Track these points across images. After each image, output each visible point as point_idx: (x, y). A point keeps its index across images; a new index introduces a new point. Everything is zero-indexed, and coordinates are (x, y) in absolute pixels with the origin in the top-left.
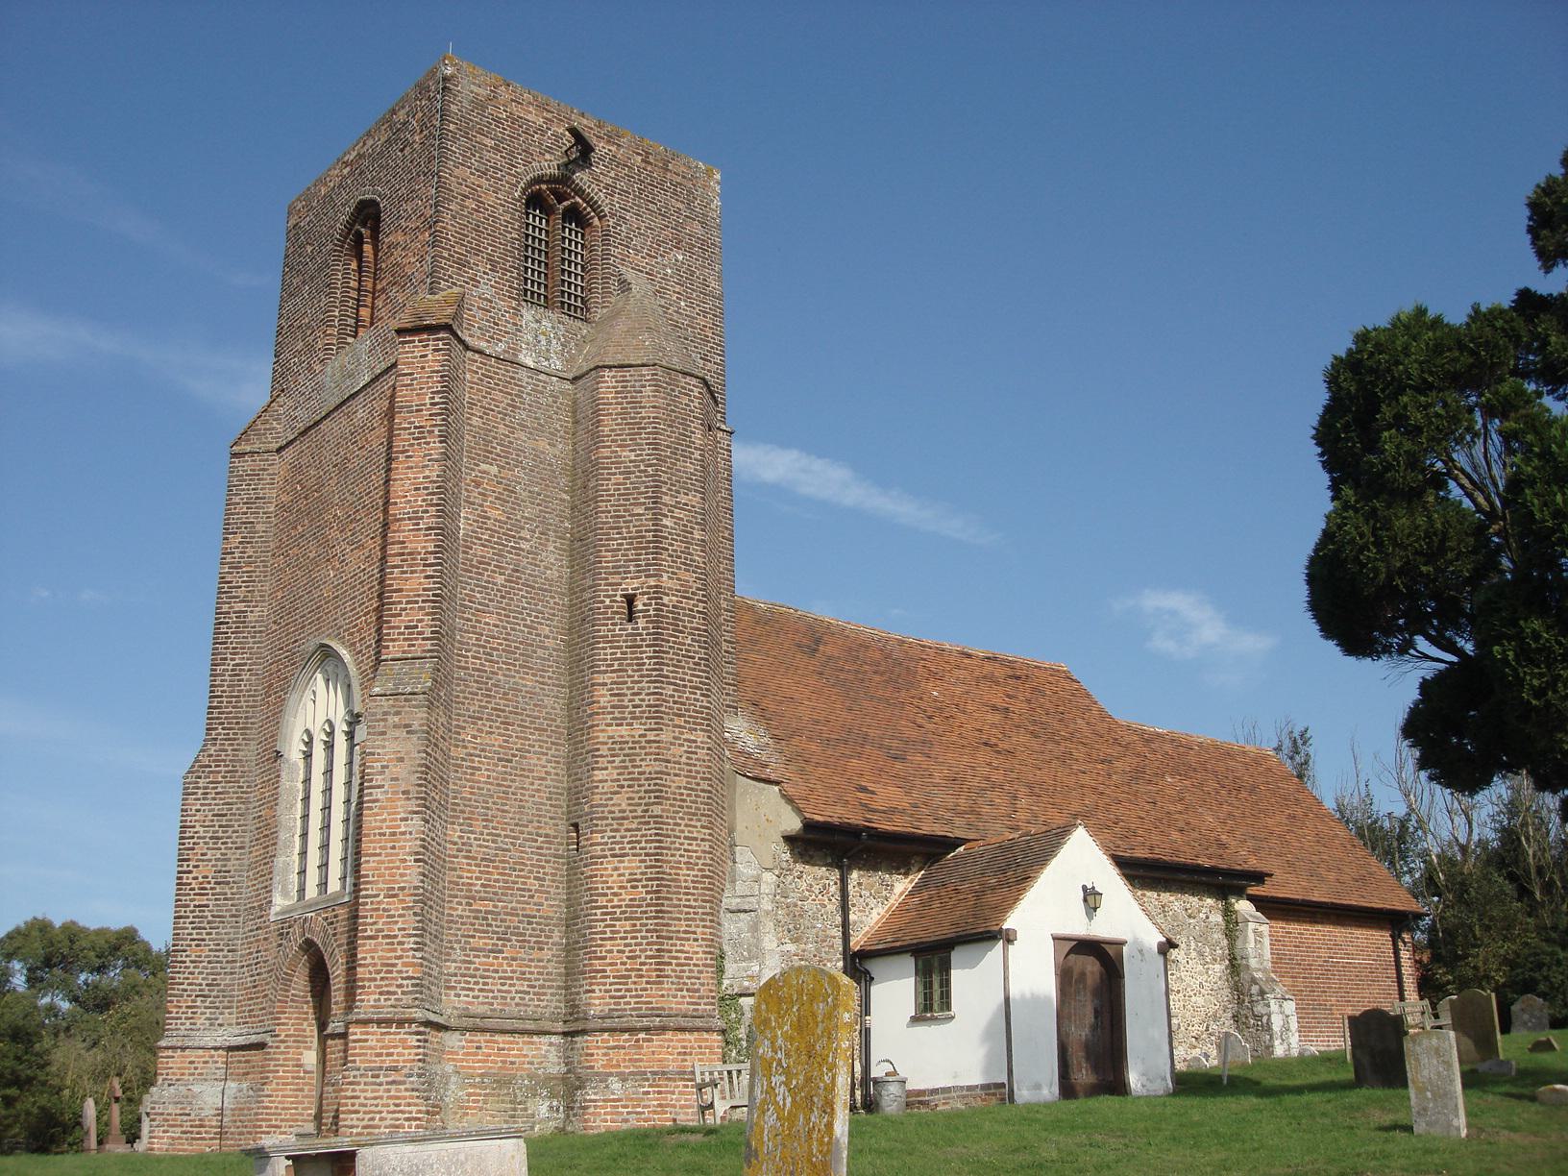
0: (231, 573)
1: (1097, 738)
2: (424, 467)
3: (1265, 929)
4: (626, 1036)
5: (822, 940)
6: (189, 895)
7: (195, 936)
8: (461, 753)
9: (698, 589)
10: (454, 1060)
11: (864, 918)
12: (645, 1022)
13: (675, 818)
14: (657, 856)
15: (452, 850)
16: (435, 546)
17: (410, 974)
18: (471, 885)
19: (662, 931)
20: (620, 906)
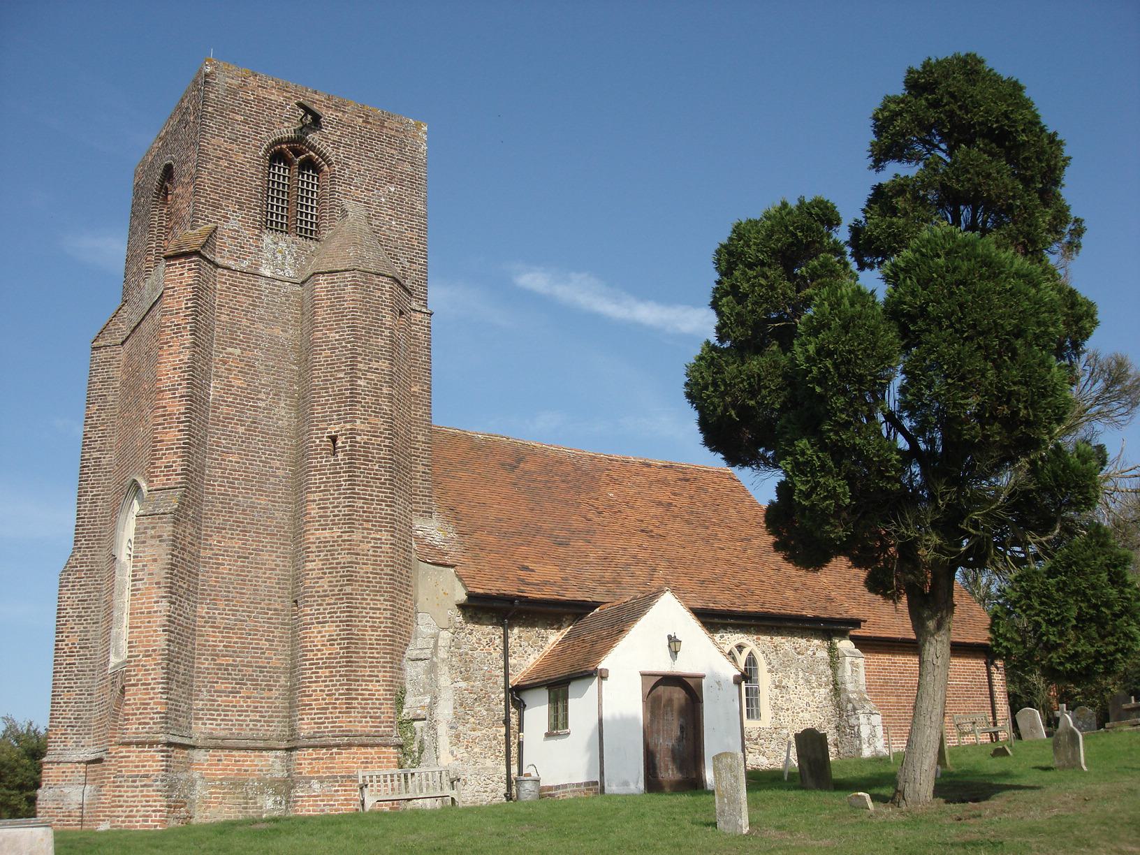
0: (91, 431)
1: (743, 523)
2: (180, 352)
3: (861, 662)
4: (324, 751)
5: (488, 678)
6: (63, 656)
7: (66, 685)
8: (209, 553)
9: (385, 429)
10: (201, 769)
11: (522, 662)
12: (338, 740)
13: (363, 595)
14: (348, 623)
15: (200, 622)
16: (186, 409)
17: (159, 710)
18: (215, 646)
19: (351, 675)
20: (322, 659)
